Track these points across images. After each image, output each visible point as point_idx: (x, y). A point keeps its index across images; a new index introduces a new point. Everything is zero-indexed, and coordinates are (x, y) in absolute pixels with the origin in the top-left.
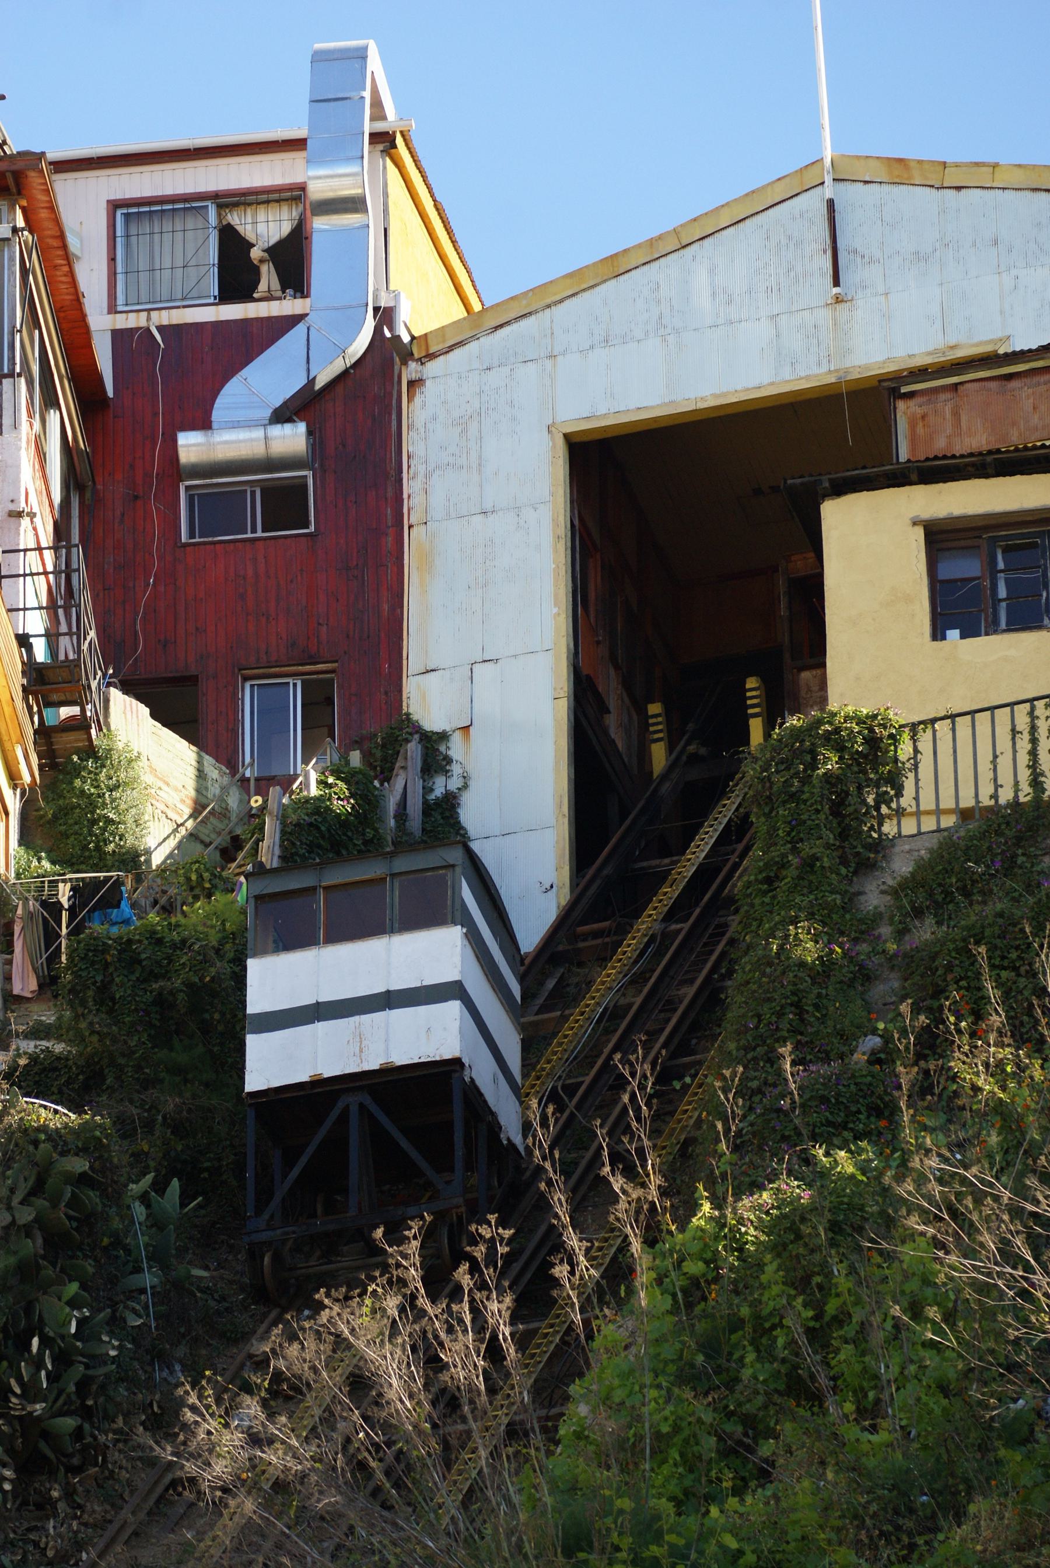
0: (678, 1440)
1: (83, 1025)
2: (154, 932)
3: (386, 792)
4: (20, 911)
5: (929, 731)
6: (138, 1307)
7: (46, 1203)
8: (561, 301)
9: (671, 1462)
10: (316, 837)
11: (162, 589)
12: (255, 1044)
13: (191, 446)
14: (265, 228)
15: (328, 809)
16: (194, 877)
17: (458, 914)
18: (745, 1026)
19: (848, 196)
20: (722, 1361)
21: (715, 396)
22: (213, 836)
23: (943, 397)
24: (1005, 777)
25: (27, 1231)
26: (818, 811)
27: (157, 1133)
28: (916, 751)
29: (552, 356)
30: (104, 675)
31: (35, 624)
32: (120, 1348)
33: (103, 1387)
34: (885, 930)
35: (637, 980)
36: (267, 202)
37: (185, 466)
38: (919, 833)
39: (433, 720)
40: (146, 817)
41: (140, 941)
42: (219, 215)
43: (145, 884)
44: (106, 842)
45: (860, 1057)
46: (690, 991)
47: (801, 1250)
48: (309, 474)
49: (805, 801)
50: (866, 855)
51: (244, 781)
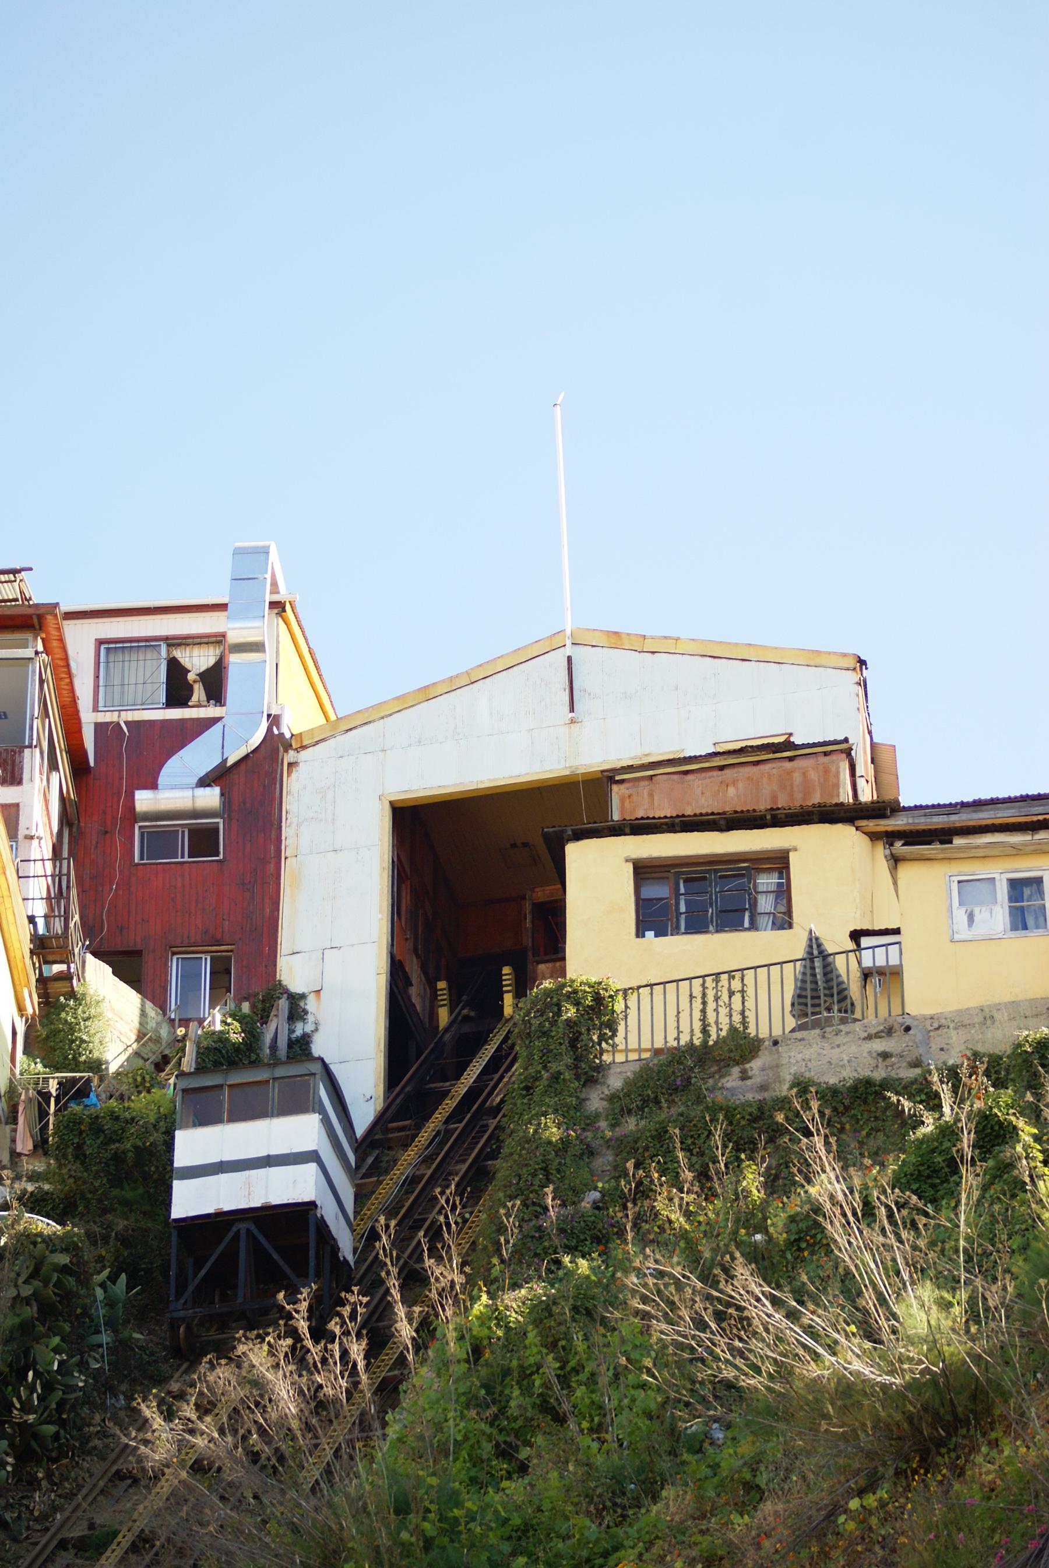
0: (467, 1445)
1: (64, 1171)
2: (114, 1112)
3: (264, 1031)
4: (23, 1097)
5: (635, 994)
6: (97, 1356)
7: (41, 1284)
8: (390, 715)
9: (462, 1459)
10: (218, 1055)
11: (121, 892)
12: (180, 1189)
13: (144, 800)
14: (197, 661)
15: (227, 1039)
16: (139, 1079)
17: (317, 1107)
18: (510, 1182)
19: (580, 655)
20: (496, 1396)
21: (490, 780)
22: (150, 1055)
23: (642, 783)
24: (685, 1027)
25: (27, 1301)
26: (561, 1044)
27: (111, 1244)
28: (627, 1007)
29: (384, 751)
30: (83, 945)
31: (39, 909)
32: (85, 1381)
33: (73, 1407)
34: (603, 1124)
35: (427, 1160)
36: (200, 644)
37: (139, 813)
38: (627, 1061)
39: (296, 986)
40: (107, 1040)
41: (104, 1117)
42: (168, 651)
43: (106, 1082)
44: (80, 1055)
45: (586, 1204)
46: (464, 1167)
47: (553, 1323)
48: (220, 821)
49: (552, 1037)
50: (591, 1074)
51: (172, 1021)
